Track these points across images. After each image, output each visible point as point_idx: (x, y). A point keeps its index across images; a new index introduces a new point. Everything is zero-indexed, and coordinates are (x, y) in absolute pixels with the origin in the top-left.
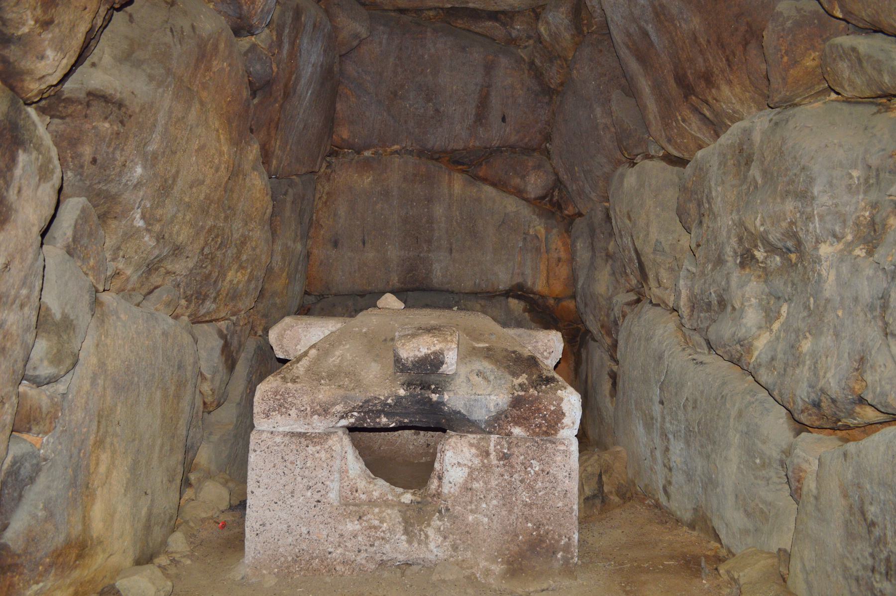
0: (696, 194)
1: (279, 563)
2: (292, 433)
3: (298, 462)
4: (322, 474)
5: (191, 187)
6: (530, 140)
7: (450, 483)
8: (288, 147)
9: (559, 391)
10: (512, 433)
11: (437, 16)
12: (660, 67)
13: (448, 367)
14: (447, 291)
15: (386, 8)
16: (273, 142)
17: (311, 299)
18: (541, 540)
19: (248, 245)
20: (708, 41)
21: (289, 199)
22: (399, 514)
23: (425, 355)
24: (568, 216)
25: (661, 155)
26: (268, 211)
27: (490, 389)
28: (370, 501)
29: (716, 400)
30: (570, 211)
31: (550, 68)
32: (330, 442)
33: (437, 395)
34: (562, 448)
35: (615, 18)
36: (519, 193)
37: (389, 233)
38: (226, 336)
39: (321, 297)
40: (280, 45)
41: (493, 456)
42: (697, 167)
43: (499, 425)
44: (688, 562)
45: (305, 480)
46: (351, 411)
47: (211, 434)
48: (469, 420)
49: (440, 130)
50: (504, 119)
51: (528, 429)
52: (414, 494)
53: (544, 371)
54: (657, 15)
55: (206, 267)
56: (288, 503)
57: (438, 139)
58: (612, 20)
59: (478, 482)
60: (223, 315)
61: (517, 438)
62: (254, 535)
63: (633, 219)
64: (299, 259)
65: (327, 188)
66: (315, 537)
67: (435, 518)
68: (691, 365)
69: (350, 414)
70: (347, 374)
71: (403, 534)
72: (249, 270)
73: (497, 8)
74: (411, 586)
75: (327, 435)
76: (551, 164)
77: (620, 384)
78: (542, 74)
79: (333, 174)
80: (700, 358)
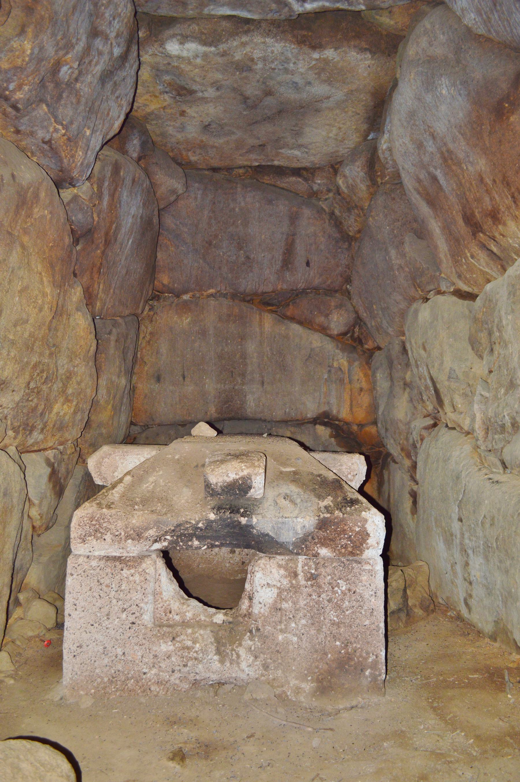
0: (487, 323)
1: (95, 684)
2: (108, 557)
3: (113, 586)
4: (136, 596)
5: (15, 326)
6: (332, 282)
7: (260, 603)
8: (112, 291)
9: (363, 513)
10: (319, 554)
11: (245, 173)
12: (449, 209)
13: (256, 491)
14: (260, 419)
15: (201, 167)
16: (96, 286)
17: (135, 429)
18: (349, 657)
19: (74, 379)
20: (494, 181)
21: (113, 338)
22: (211, 635)
23: (234, 480)
24: (368, 350)
25: (452, 290)
26: (92, 348)
27: (297, 512)
28: (183, 622)
29: (513, 517)
30: (369, 345)
31: (349, 217)
32: (144, 565)
33: (246, 519)
34: (368, 567)
35: (406, 166)
36: (323, 330)
37: (206, 368)
38: (53, 464)
39: (146, 427)
40: (100, 196)
41: (301, 577)
42: (486, 299)
43: (306, 547)
44: (492, 675)
45: (120, 603)
46: (163, 535)
47: (40, 555)
48: (277, 543)
49: (251, 274)
50: (308, 264)
51: (334, 550)
52: (226, 614)
53: (349, 494)
54: (445, 160)
55: (32, 401)
56: (104, 625)
57: (249, 283)
58: (403, 168)
59: (287, 602)
60: (50, 444)
61: (323, 558)
62: (72, 657)
63: (428, 349)
64: (124, 392)
65: (150, 329)
66: (130, 658)
67: (246, 637)
68: (488, 484)
69: (163, 538)
70: (160, 500)
71: (216, 654)
72: (74, 403)
73: (299, 165)
74: (223, 706)
75: (142, 558)
76: (351, 303)
77: (420, 503)
78: (341, 223)
79: (156, 316)
80: (496, 477)
